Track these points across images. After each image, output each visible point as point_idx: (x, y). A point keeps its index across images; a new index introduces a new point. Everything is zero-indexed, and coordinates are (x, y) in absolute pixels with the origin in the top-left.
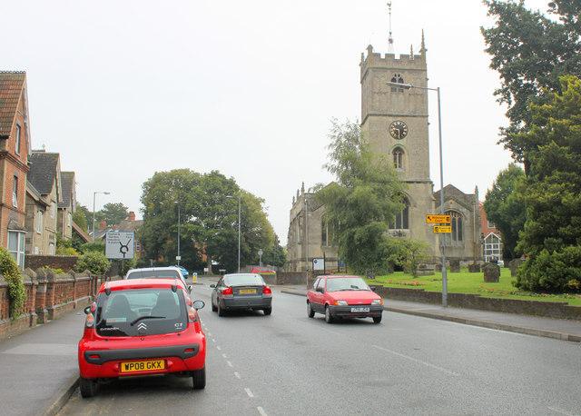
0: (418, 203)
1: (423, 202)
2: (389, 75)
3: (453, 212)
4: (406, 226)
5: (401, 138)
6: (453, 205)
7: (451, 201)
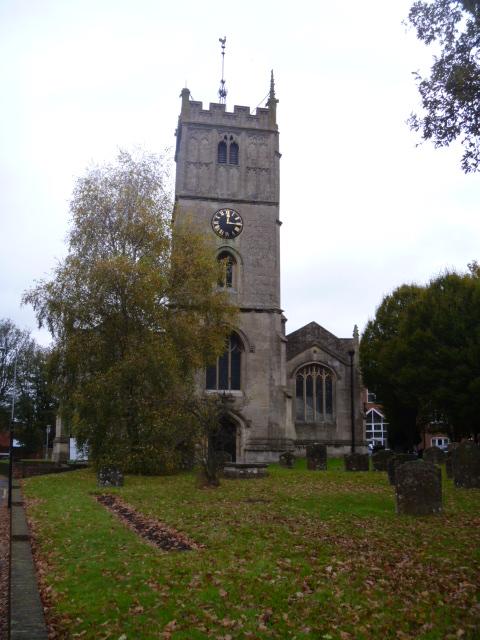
0: (257, 348)
1: (266, 345)
2: (215, 137)
3: (317, 365)
4: (236, 386)
5: (232, 237)
6: (317, 355)
7: (315, 348)
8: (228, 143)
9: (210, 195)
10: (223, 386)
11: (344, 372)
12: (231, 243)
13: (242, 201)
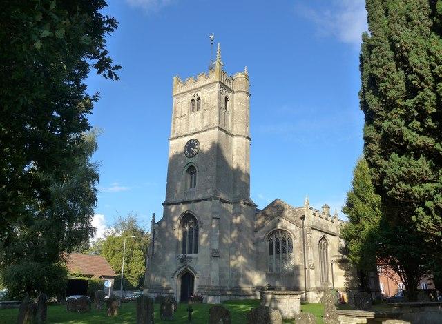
4: (196, 252)
8: (195, 99)
9: (186, 133)
10: (190, 252)
11: (298, 233)
12: (194, 160)
13: (199, 132)
